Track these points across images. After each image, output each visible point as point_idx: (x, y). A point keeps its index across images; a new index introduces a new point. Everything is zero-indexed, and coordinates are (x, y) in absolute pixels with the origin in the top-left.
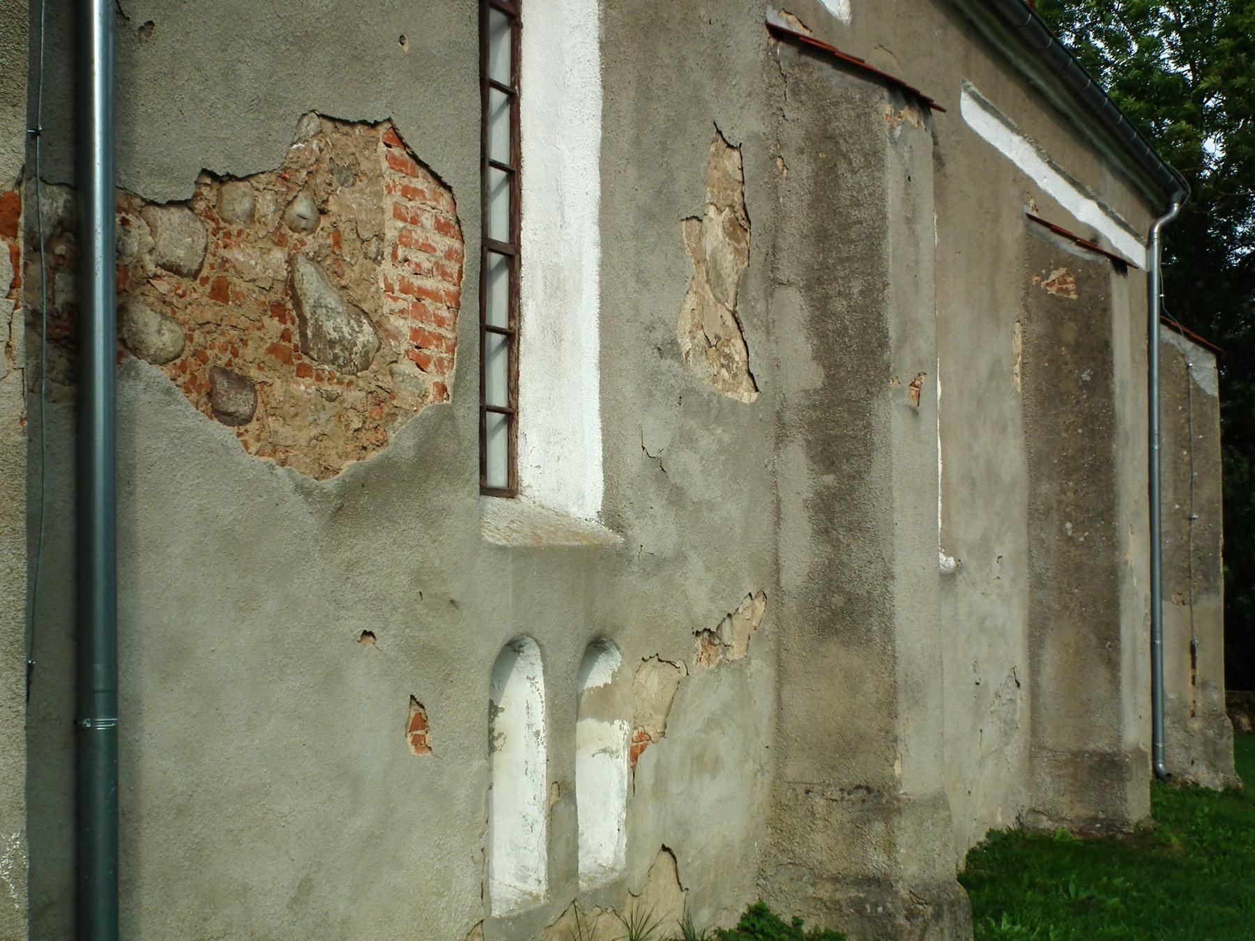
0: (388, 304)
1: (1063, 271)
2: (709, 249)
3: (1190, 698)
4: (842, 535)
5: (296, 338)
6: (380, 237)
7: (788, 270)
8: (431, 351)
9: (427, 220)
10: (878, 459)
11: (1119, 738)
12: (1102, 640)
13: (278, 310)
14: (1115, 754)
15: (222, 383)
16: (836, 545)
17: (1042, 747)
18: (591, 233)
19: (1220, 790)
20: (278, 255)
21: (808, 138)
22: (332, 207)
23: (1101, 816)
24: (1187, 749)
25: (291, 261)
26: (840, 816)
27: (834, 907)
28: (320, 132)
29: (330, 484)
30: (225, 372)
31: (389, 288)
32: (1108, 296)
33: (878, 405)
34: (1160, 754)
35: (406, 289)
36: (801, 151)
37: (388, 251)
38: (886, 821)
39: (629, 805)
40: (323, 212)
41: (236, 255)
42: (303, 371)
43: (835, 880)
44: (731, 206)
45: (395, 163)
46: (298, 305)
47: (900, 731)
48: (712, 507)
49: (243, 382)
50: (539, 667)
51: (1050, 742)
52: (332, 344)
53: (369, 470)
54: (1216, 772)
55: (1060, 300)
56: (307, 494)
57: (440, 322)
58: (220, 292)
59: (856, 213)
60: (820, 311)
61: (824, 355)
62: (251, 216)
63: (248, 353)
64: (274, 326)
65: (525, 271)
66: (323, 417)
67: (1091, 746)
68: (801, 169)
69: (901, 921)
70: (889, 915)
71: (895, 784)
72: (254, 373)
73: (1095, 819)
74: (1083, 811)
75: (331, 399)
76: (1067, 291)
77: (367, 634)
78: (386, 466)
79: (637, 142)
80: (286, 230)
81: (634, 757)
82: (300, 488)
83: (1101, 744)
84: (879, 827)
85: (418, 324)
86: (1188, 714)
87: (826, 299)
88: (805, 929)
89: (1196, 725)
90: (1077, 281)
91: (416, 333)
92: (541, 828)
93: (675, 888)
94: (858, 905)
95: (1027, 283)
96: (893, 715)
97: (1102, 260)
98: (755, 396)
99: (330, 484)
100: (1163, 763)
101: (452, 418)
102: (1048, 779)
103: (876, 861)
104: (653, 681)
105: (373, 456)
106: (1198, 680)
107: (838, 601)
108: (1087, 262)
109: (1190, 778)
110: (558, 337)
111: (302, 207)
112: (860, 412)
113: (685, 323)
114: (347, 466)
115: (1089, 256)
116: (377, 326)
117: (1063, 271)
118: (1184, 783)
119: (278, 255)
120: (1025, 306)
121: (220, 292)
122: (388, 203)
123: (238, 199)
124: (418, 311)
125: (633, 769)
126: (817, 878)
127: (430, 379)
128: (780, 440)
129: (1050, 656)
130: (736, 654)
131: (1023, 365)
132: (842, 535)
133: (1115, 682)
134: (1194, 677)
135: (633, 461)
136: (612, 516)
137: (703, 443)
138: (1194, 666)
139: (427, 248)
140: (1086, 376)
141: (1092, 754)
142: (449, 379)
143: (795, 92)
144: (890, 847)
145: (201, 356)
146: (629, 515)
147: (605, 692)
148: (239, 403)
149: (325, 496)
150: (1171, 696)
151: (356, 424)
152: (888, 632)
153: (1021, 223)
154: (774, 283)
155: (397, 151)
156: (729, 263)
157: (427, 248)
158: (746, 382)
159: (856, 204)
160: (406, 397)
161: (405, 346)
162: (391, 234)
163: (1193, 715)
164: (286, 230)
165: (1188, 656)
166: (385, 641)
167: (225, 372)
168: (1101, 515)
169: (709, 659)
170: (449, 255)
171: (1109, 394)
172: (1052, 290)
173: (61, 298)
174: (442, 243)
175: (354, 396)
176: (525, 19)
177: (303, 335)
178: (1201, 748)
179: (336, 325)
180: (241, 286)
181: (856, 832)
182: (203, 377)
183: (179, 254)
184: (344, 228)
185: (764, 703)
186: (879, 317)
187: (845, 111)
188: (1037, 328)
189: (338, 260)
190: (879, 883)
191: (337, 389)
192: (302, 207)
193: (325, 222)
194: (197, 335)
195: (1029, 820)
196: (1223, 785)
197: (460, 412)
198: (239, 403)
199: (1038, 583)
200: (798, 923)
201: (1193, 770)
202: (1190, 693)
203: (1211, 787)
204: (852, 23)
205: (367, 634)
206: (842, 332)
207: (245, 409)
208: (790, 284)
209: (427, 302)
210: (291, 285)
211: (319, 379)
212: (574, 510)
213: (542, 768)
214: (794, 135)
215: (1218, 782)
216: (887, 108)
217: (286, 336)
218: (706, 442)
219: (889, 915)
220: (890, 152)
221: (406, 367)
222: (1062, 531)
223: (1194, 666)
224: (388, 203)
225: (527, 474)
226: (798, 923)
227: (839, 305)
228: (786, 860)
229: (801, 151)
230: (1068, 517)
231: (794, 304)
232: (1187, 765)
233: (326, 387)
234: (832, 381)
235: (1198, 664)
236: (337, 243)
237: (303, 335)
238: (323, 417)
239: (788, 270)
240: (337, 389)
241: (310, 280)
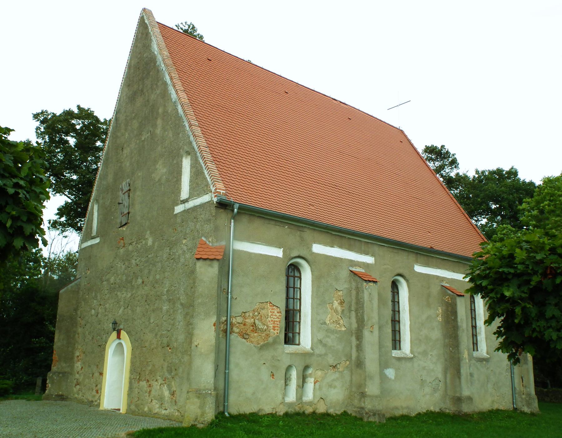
0: (269, 323)
1: (448, 296)
2: (335, 307)
3: (522, 390)
4: (359, 351)
5: (255, 329)
6: (268, 315)
7: (353, 308)
8: (276, 328)
9: (276, 312)
10: (364, 339)
11: (461, 394)
12: (458, 373)
13: (253, 326)
14: (460, 397)
15: (244, 335)
16: (359, 353)
17: (447, 395)
18: (310, 308)
19: (529, 413)
20: (253, 320)
21: (355, 288)
22: (261, 313)
23: (458, 410)
24: (522, 402)
25: (254, 320)
26: (358, 397)
27: (356, 412)
28: (259, 305)
29: (259, 346)
30: (245, 334)
31: (269, 321)
32: (456, 302)
33: (364, 331)
34: (515, 403)
35: (272, 321)
36: (354, 290)
37: (269, 317)
38: (364, 398)
39: (314, 390)
40: (259, 314)
41: (247, 321)
42: (256, 332)
43: (357, 408)
44: (340, 300)
45: (270, 306)
46: (255, 325)
47: (367, 383)
48: (334, 347)
49: (247, 334)
50: (295, 369)
51: (449, 394)
52: (260, 329)
53: (265, 343)
54: (529, 408)
55: (448, 302)
56: (255, 347)
57: (277, 324)
58: (245, 325)
59: (361, 300)
60: (357, 314)
61: (357, 322)
62: (249, 316)
63: (248, 331)
64: (252, 328)
65: (301, 313)
66: (258, 338)
67: (456, 395)
68: (354, 293)
69: (364, 414)
70: (363, 413)
71: (366, 392)
72: (249, 333)
73: (457, 411)
74: (455, 409)
75: (260, 335)
76: (449, 301)
77: (264, 364)
78: (268, 343)
79: (317, 295)
80: (254, 316)
81: (315, 383)
82: (254, 346)
83: (458, 395)
84: (363, 399)
85: (274, 325)
86: (522, 394)
87: (357, 313)
88: (352, 415)
89: (524, 396)
90: (451, 299)
91: (273, 326)
92: (295, 392)
93: (324, 405)
94: (359, 411)
95: (442, 299)
96: (366, 381)
97: (455, 294)
98: (345, 329)
99: (259, 346)
100: (516, 405)
101: (279, 337)
102: (448, 402)
103: (363, 405)
104: (319, 373)
105: (266, 342)
106: (524, 385)
107: (359, 362)
108: (452, 295)
109: (522, 410)
110: (305, 322)
111: (256, 314)
112: (361, 332)
113: (328, 319)
114: (262, 343)
115: (452, 294)
116: (267, 326)
117: (448, 296)
118: (521, 411)
119: (253, 320)
120: (442, 303)
121: (245, 325)
122: (269, 311)
123: (247, 314)
124: (274, 323)
125: (314, 385)
126: (355, 407)
127: (276, 332)
128: (352, 335)
129: (449, 376)
130: (341, 370)
131: (442, 315)
132: (359, 351)
133: (460, 382)
134: (523, 385)
135: (315, 340)
136: (312, 348)
137: (332, 337)
138: (523, 382)
139: (276, 315)
140: (453, 318)
141: (457, 397)
142: (278, 332)
143: (354, 280)
144: (364, 403)
145: (242, 332)
146: (315, 348)
147: (311, 374)
148: (247, 337)
149: (258, 347)
150: (518, 389)
151: (263, 338)
152: (365, 367)
153: (439, 288)
154: (350, 311)
155: (271, 304)
156: (339, 309)
157: (276, 315)
158: (343, 327)
159: (361, 299)
160: (272, 334)
161: (272, 328)
162: (270, 315)
163: (523, 394)
164: (254, 316)
165: (521, 380)
166: (267, 364)
167: (245, 334)
168: (456, 347)
169: (334, 370)
170: (279, 316)
171: (457, 322)
172: (447, 300)
173: (225, 328)
174: (278, 315)
175: (263, 335)
176: (302, 278)
177: (256, 328)
178: (525, 402)
179: (261, 326)
180: (247, 324)
181: (360, 400)
182: (242, 334)
183: (239, 321)
184: (263, 316)
185: (348, 378)
186: (364, 317)
187: (360, 284)
188: (444, 308)
189: (261, 319)
190: (363, 408)
191: (261, 334)
192: (256, 314)
193: (260, 315)
194: (241, 330)
195: (444, 410)
196: (530, 411)
197: (280, 336)
198: (247, 337)
199: (446, 360)
200: (351, 414)
201: (523, 408)
202: (522, 389)
203: (528, 412)
204: (375, 263)
205: (264, 364)
206: (359, 319)
207: (248, 337)
208: (353, 311)
209: (275, 322)
210: (254, 323)
211: (258, 333)
212: (307, 347)
213: (296, 383)
214: (354, 287)
215: (529, 411)
216: (365, 284)
217: (253, 329)
218: (332, 337)
219: (363, 413)
220: (365, 291)
221: (272, 331)
222: (450, 349)
223: (523, 382)
224: (269, 311)
225: (301, 342)
226: (351, 414)
227: (359, 314)
228: (351, 404)
229: (354, 290)
230: (451, 347)
231: (353, 313)
232: (522, 406)
233: (259, 334)
234: (358, 327)
235: (524, 381)
236: (261, 317)
237: (256, 328)
238: (258, 338)
239: (353, 308)
240: (261, 334)
241: (257, 322)
